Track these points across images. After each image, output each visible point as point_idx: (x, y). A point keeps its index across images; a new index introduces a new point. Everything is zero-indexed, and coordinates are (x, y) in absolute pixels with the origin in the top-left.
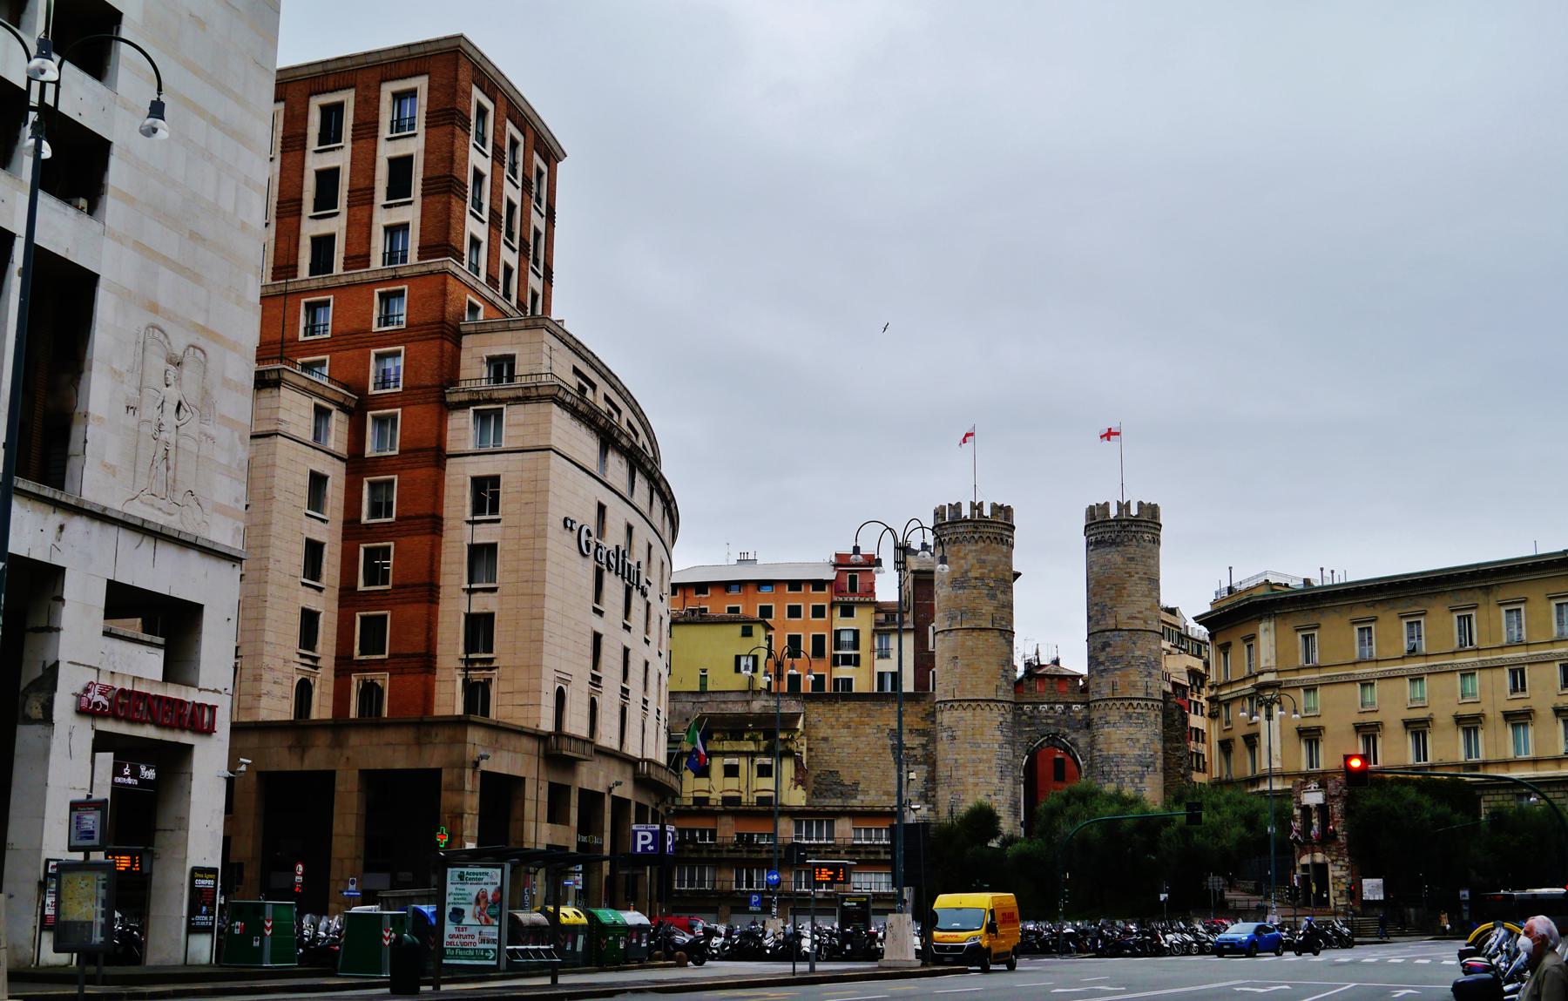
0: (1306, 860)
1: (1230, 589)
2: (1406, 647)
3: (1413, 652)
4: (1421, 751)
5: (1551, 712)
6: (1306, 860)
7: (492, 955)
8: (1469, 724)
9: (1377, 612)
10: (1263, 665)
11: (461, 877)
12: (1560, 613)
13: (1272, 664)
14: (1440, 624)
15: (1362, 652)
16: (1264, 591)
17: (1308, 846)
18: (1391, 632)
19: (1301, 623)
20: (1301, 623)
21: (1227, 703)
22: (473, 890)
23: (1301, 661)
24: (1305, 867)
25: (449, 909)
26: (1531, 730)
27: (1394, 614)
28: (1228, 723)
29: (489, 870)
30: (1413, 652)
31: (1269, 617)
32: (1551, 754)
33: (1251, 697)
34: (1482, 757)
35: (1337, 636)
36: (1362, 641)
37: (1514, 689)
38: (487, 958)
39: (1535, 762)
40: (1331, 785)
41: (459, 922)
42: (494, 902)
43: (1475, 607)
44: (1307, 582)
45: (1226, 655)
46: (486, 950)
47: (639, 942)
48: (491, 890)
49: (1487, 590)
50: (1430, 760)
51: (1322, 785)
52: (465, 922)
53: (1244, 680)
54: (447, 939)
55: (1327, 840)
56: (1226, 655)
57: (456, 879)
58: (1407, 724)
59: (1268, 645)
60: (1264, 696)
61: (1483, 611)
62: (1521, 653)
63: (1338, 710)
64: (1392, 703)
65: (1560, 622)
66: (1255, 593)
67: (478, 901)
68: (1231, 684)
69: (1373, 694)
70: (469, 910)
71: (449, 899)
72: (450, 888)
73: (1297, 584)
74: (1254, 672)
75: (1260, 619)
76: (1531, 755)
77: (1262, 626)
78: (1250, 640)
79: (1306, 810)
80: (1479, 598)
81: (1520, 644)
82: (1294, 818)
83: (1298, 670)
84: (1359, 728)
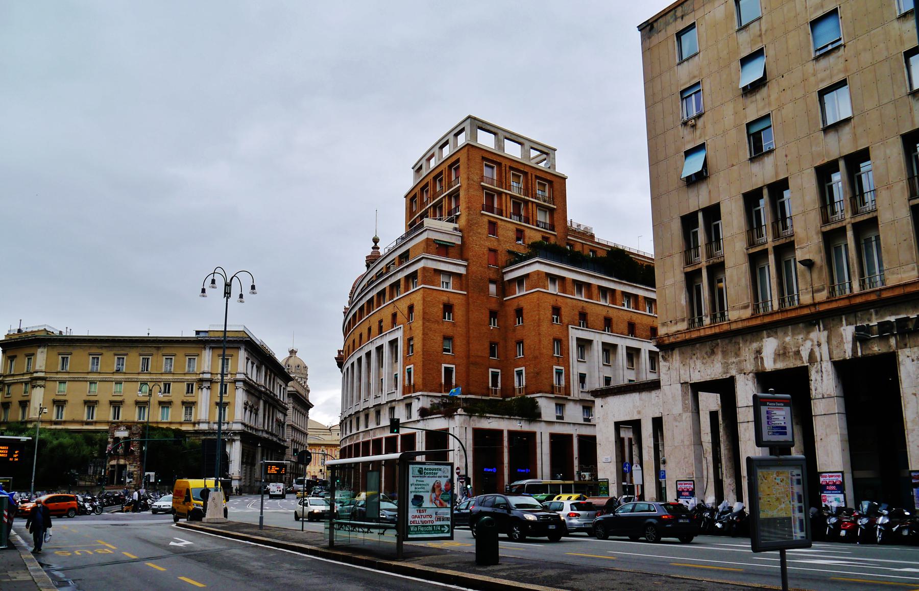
0: (113, 462)
1: (19, 331)
2: (115, 369)
3: (118, 371)
4: (116, 415)
5: (180, 403)
6: (113, 462)
7: (446, 529)
8: (142, 405)
9: (103, 351)
10: (37, 368)
11: (420, 471)
12: (189, 362)
13: (43, 369)
14: (134, 360)
15: (93, 368)
16: (43, 334)
17: (116, 456)
18: (109, 361)
19: (61, 351)
20: (61, 351)
21: (9, 385)
22: (430, 482)
23: (59, 369)
24: (113, 466)
25: (411, 497)
26: (170, 410)
27: (111, 353)
28: (8, 394)
29: (442, 467)
30: (118, 371)
31: (44, 346)
32: (178, 420)
33: (26, 383)
34: (64, 419)
35: (80, 359)
36: (93, 364)
37: (188, 392)
38: (443, 532)
39: (171, 423)
40: (134, 428)
41: (420, 506)
42: (447, 490)
43: (152, 355)
44: (61, 332)
45: (11, 362)
46: (442, 526)
47: (683, 518)
48: (443, 482)
49: (158, 348)
50: (120, 419)
51: (128, 428)
52: (425, 505)
53: (23, 374)
54: (410, 519)
55: (128, 454)
56: (11, 362)
57: (417, 473)
58: (111, 402)
59: (41, 359)
60: (33, 382)
61: (155, 357)
62: (170, 377)
63: (75, 393)
64: (104, 392)
65: (189, 366)
66: (37, 334)
67: (434, 490)
68: (13, 375)
69: (95, 388)
70: (427, 497)
71: (411, 488)
72: (412, 480)
73: (57, 333)
74: (31, 371)
75: (39, 347)
76: (169, 420)
77: (40, 350)
78: (30, 356)
79: (117, 439)
80: (154, 351)
81: (170, 373)
82: (108, 443)
83: (57, 373)
84: (86, 402)
